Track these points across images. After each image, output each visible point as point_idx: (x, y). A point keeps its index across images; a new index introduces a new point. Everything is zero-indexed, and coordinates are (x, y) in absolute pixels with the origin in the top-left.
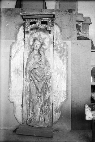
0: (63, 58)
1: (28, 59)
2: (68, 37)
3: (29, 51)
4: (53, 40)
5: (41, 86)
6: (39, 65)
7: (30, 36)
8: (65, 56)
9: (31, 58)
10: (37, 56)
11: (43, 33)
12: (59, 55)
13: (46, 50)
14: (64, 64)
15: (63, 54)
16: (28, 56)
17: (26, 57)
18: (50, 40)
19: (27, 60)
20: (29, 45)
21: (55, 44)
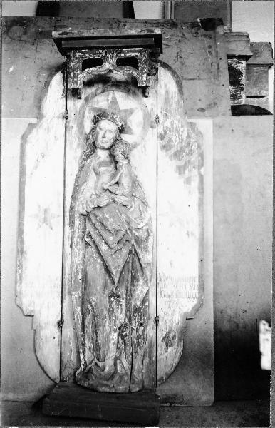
0: (187, 172)
1: (78, 177)
3: (79, 152)
5: (121, 262)
7: (83, 106)
9: (87, 174)
15: (189, 161)
16: (77, 169)
17: (73, 169)
18: (147, 116)
19: (76, 181)
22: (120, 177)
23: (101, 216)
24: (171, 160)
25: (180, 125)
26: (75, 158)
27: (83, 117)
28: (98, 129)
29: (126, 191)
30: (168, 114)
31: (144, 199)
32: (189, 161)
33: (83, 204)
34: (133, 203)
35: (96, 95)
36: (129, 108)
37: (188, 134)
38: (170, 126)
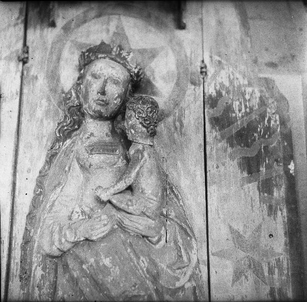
0: (263, 169)
1: (42, 175)
2: (275, 59)
3: (50, 127)
4: (199, 64)
6: (119, 215)
7: (59, 41)
8: (276, 161)
9: (64, 171)
10: (102, 157)
11: (140, 23)
12: (241, 152)
13: (160, 120)
14: (272, 210)
15: (266, 148)
16: (43, 159)
17: (34, 159)
18: (183, 63)
19: (40, 184)
20: (56, 91)
21: (211, 91)
22: (138, 173)
23: (92, 260)
24: (232, 146)
25: (246, 82)
26: (40, 137)
27: (59, 59)
28: (89, 77)
29: (153, 204)
30: (224, 62)
31: (185, 222)
32: (266, 148)
33: (52, 233)
34: (163, 232)
35: (85, 22)
36: (148, 46)
37: (261, 98)
38: (227, 84)
